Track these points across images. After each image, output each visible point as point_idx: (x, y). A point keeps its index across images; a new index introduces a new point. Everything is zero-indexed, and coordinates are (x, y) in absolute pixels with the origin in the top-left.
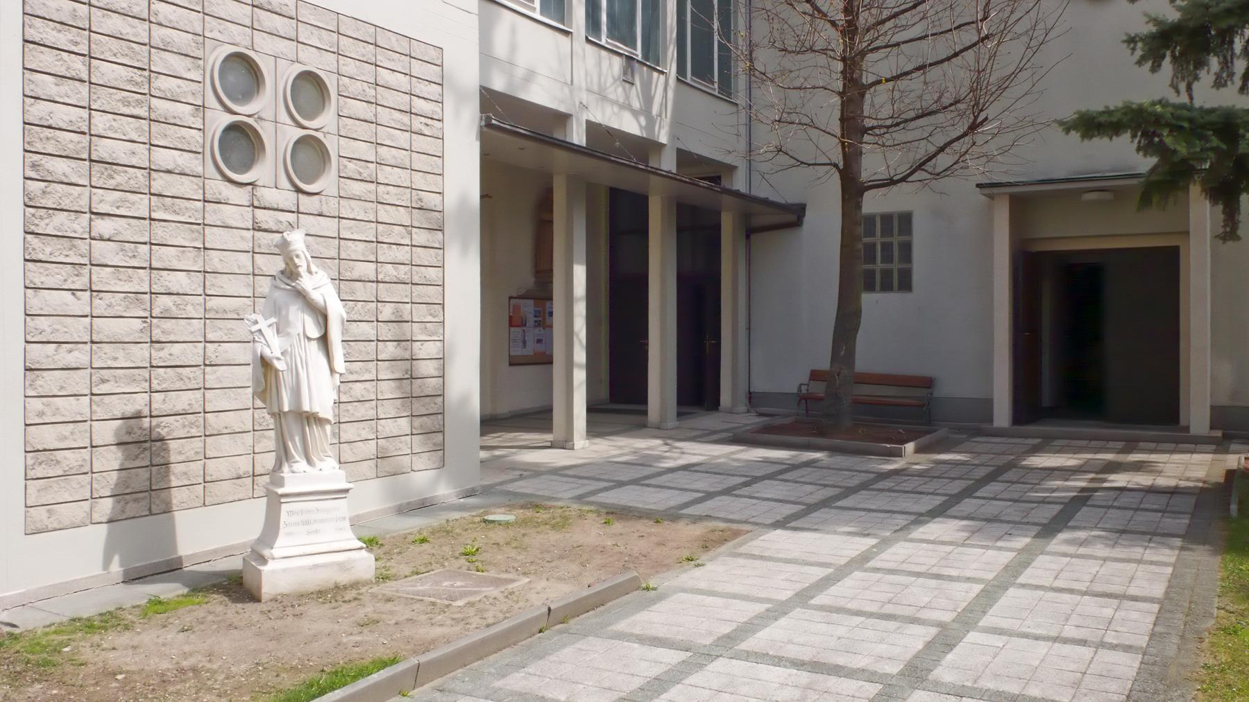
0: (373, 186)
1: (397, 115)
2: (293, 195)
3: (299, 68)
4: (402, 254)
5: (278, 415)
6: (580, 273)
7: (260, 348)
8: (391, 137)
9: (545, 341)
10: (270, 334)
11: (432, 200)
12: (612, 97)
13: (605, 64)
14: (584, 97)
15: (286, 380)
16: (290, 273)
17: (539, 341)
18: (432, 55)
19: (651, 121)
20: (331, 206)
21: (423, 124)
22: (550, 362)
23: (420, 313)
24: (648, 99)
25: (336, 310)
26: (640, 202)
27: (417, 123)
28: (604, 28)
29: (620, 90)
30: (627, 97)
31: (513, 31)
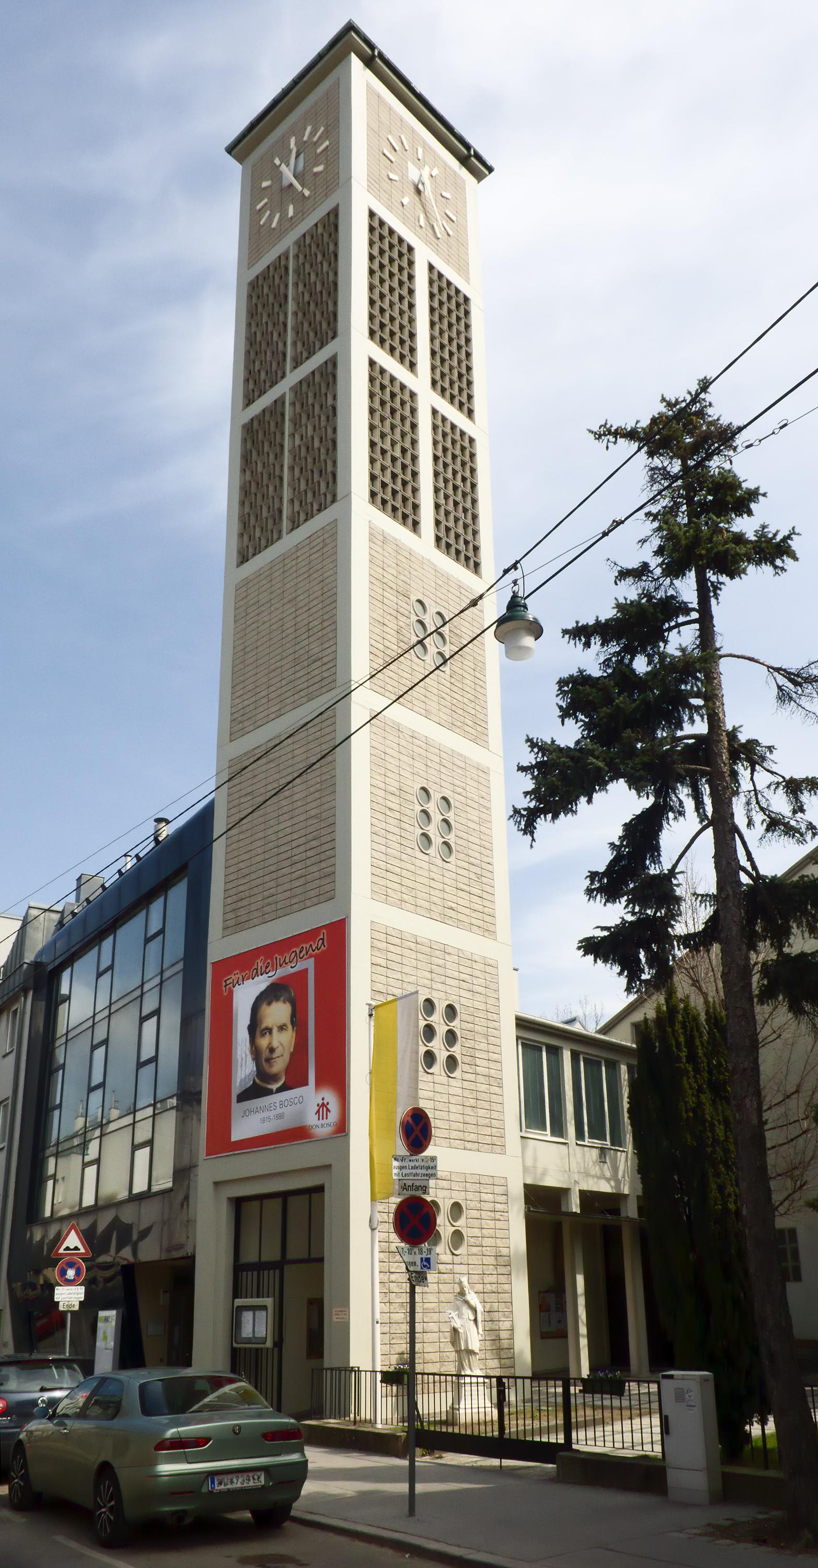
0: (480, 1248)
1: (489, 1213)
2: (451, 1257)
3: (453, 1201)
4: (493, 1279)
5: (458, 1352)
6: (580, 1280)
7: (453, 1324)
8: (487, 1224)
9: (563, 1321)
10: (456, 1318)
11: (505, 1251)
12: (593, 1173)
13: (587, 1155)
14: (576, 1177)
15: (462, 1337)
16: (462, 1293)
17: (559, 1322)
18: (503, 1182)
19: (618, 1182)
20: (465, 1260)
21: (499, 1215)
22: (566, 1337)
23: (502, 1307)
24: (615, 1169)
25: (480, 1309)
26: (618, 1229)
27: (498, 1215)
28: (587, 1134)
29: (597, 1168)
30: (602, 1170)
31: (535, 1150)
